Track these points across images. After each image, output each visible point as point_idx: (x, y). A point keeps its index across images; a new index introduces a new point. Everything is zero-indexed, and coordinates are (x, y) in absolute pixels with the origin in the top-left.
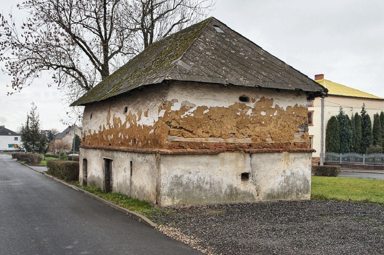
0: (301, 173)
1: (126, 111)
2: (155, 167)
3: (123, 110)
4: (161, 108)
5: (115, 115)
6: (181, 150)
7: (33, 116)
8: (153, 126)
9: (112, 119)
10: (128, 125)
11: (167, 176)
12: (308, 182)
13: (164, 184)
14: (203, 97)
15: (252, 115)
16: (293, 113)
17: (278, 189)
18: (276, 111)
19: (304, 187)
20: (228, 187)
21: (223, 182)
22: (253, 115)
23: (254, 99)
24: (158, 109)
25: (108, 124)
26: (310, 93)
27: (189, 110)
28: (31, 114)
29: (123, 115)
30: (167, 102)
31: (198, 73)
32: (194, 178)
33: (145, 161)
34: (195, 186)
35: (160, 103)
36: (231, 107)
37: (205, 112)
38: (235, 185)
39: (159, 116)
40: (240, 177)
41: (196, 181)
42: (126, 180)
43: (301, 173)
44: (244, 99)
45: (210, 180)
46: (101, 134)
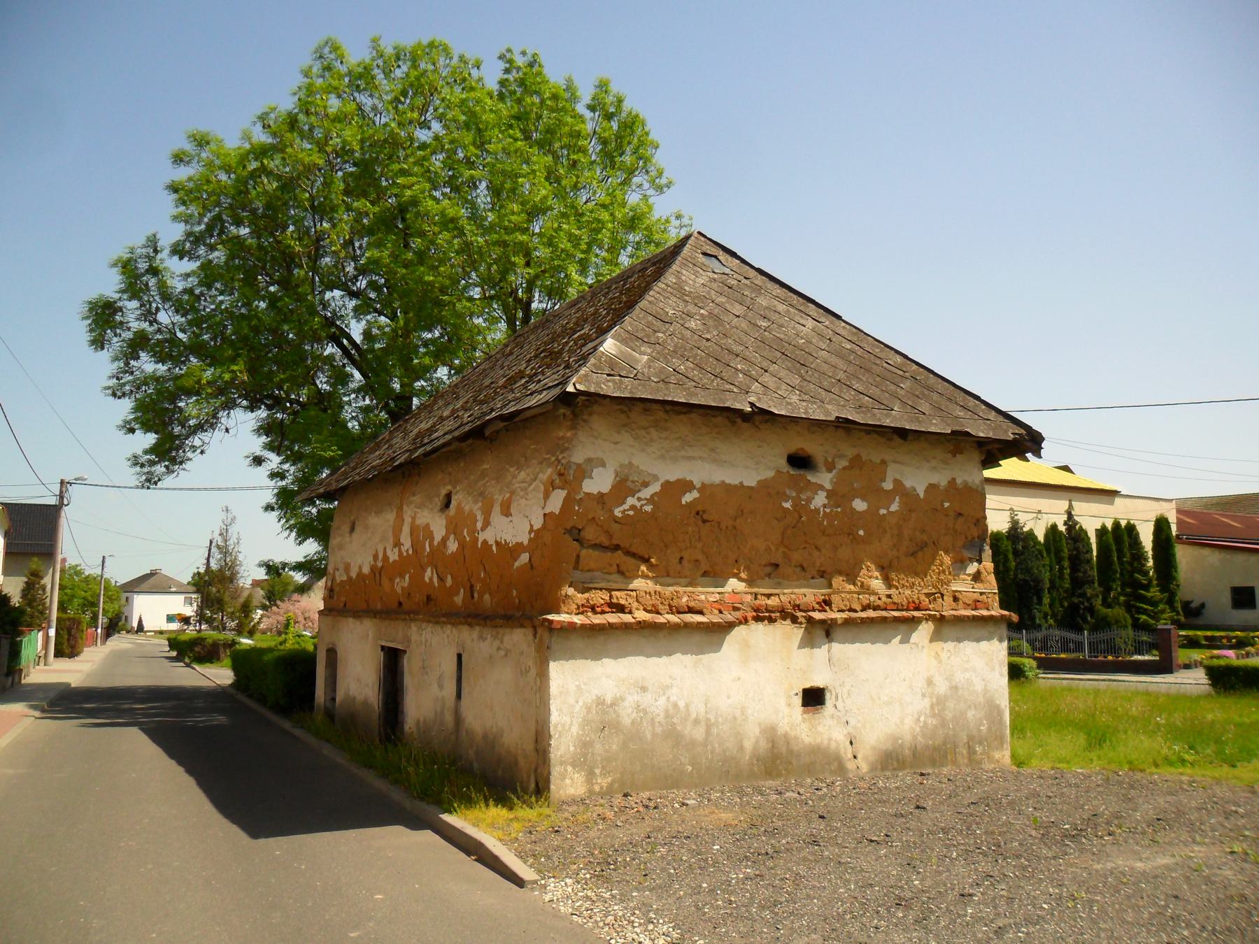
0: (979, 687)
1: (447, 505)
2: (533, 672)
3: (438, 502)
4: (551, 486)
5: (415, 515)
6: (613, 618)
7: (226, 541)
8: (526, 542)
9: (406, 529)
10: (453, 546)
11: (571, 701)
12: (1000, 713)
13: (560, 728)
14: (680, 451)
15: (828, 510)
16: (946, 505)
17: (915, 738)
18: (897, 498)
19: (989, 729)
20: (763, 731)
21: (747, 717)
22: (831, 511)
23: (830, 460)
24: (542, 488)
25: (397, 544)
26: (990, 447)
27: (640, 491)
28: (220, 535)
29: (440, 514)
30: (570, 467)
31: (663, 377)
32: (658, 706)
33: (502, 653)
34: (659, 730)
35: (549, 471)
36: (763, 484)
37: (688, 498)
38: (783, 727)
39: (547, 511)
40: (798, 701)
41: (662, 715)
42: (442, 712)
43: (979, 687)
44: (800, 461)
45: (706, 712)
46: (377, 575)
